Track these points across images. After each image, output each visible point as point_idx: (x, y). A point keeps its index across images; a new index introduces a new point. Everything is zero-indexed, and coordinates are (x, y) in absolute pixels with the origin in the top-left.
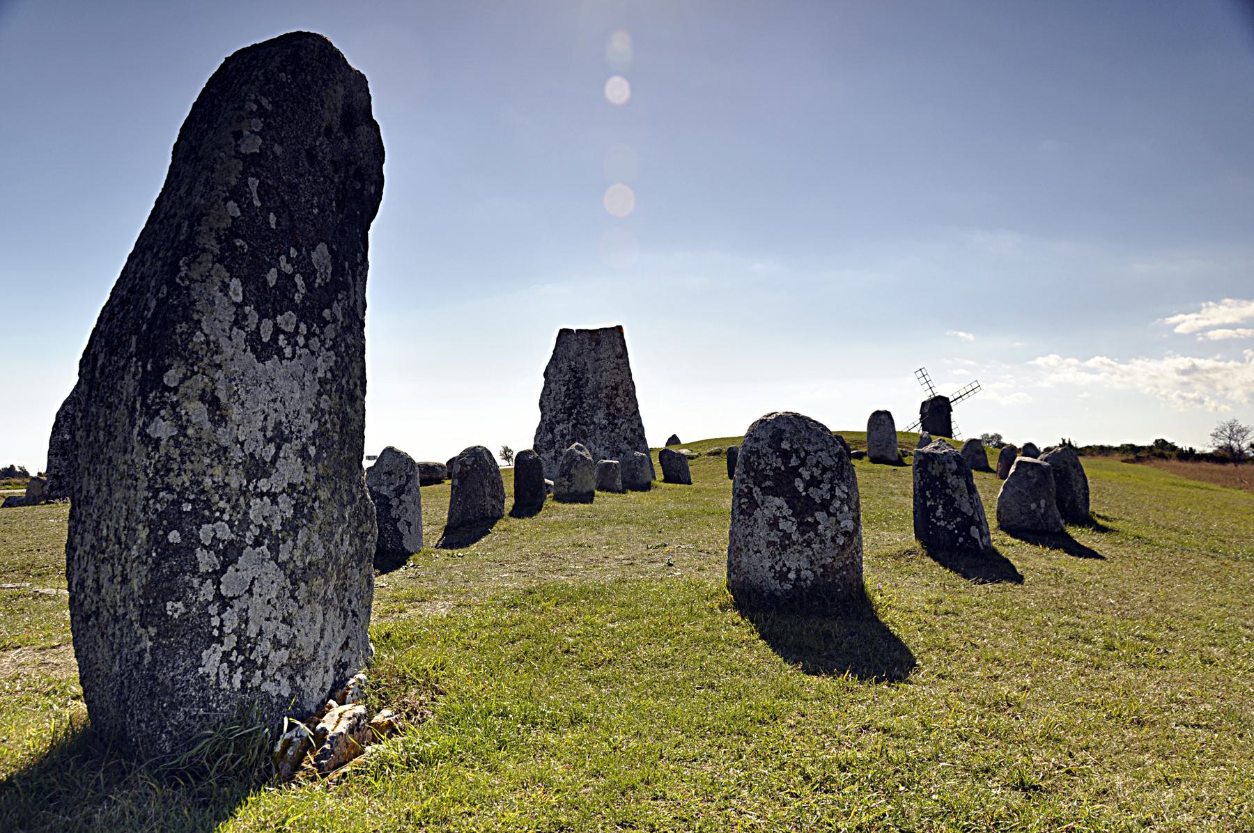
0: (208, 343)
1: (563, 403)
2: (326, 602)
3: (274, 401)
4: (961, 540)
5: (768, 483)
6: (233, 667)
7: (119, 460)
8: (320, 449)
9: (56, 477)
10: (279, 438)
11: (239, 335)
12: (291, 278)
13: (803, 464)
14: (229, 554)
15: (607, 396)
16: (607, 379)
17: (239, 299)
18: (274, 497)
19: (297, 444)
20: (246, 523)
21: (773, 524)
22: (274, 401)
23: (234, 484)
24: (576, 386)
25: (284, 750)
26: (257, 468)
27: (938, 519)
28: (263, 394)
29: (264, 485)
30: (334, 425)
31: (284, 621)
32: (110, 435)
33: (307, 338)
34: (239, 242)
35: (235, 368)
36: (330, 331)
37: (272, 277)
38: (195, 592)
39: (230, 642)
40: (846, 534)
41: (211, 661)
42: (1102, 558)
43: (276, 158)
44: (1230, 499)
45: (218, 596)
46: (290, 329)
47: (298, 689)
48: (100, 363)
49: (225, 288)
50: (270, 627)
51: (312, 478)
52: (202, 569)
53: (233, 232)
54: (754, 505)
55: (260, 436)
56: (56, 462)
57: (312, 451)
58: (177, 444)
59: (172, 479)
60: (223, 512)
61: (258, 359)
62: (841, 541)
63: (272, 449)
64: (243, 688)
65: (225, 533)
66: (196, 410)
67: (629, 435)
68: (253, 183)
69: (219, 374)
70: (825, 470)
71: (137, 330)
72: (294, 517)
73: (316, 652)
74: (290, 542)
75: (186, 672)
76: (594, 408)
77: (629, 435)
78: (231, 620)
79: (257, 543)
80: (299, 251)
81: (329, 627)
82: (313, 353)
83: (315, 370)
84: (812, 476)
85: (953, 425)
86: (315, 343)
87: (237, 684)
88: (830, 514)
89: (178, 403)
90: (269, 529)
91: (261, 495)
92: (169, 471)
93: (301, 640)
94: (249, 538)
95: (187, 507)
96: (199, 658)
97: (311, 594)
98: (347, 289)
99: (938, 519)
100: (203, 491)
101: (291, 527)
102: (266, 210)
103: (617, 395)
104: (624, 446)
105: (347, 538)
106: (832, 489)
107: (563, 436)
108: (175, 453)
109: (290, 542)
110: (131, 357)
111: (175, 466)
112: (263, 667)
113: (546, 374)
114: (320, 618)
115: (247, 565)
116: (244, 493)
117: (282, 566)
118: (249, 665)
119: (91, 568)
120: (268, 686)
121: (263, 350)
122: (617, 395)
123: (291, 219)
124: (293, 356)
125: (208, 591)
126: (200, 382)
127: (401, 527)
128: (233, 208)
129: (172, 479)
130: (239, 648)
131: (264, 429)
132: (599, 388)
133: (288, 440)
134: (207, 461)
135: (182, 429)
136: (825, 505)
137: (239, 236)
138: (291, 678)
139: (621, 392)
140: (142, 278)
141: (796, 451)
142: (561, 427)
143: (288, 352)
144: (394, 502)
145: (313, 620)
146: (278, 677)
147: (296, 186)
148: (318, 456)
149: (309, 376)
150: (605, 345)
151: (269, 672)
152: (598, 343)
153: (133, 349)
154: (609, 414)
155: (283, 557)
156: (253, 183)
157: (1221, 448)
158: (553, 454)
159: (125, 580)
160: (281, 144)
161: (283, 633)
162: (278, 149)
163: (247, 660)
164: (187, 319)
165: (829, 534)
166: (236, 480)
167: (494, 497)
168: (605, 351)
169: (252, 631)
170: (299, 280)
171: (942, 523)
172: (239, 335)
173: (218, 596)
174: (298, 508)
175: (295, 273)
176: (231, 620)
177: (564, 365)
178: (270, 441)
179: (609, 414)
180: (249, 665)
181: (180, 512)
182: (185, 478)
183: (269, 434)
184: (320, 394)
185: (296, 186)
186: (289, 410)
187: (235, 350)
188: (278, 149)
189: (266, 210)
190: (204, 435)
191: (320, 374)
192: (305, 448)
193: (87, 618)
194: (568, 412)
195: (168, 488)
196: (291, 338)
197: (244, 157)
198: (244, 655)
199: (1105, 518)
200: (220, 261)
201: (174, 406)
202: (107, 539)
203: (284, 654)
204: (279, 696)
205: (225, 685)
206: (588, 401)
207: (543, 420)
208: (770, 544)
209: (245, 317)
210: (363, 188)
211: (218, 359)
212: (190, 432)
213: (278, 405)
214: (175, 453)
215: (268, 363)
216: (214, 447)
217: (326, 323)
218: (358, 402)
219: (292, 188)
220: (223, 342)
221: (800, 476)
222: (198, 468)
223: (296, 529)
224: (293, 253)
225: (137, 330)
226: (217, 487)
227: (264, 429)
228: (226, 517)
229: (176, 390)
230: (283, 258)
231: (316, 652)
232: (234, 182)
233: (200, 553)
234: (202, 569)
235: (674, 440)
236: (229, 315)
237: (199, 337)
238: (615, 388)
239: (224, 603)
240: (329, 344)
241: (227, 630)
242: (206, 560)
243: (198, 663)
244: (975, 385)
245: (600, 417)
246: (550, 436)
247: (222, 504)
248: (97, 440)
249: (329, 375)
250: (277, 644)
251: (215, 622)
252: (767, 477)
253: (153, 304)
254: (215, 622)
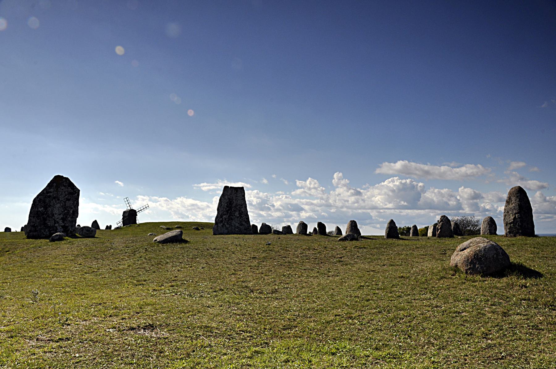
9: (33, 226)
42: (537, 275)
56: (32, 218)
77: (245, 220)
107: (225, 219)
132: (237, 205)
142: (225, 216)
152: (237, 191)
157: (380, 167)
158: (222, 224)
177: (226, 197)
194: (227, 211)
199: (548, 218)
206: (233, 209)
218: (220, 213)
238: (242, 205)
245: (237, 214)
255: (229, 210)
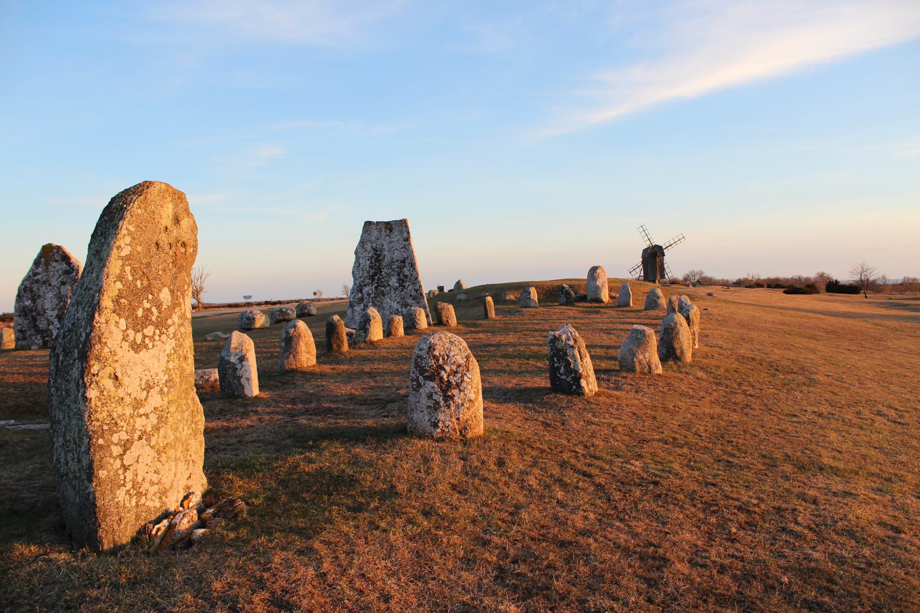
1: (368, 272)
2: (176, 459)
4: (574, 387)
5: (427, 374)
7: (73, 406)
10: (148, 388)
11: (126, 345)
12: (149, 310)
14: (126, 446)
15: (398, 267)
16: (397, 255)
17: (124, 328)
18: (147, 416)
19: (157, 389)
20: (134, 430)
21: (430, 396)
23: (128, 414)
24: (377, 260)
25: (157, 532)
26: (138, 404)
27: (562, 375)
28: (139, 369)
29: (142, 411)
30: (176, 374)
31: (155, 472)
32: (68, 395)
33: (160, 336)
34: (123, 301)
35: (125, 361)
36: (172, 330)
37: (140, 313)
38: (112, 465)
39: (129, 485)
41: (121, 494)
43: (139, 253)
44: (904, 298)
45: (123, 466)
46: (151, 334)
47: (164, 503)
48: (61, 359)
50: (148, 477)
51: (166, 403)
52: (115, 454)
53: (120, 296)
54: (419, 386)
55: (139, 389)
57: (166, 389)
58: (100, 400)
60: (122, 427)
61: (136, 352)
63: (145, 393)
64: (137, 506)
65: (124, 436)
66: (108, 383)
67: (413, 293)
68: (128, 269)
69: (117, 365)
71: (77, 347)
72: (158, 423)
73: (172, 484)
76: (389, 275)
77: (413, 293)
78: (129, 475)
79: (140, 438)
80: (153, 295)
81: (179, 471)
84: (451, 370)
85: (665, 266)
86: (164, 337)
87: (134, 504)
88: (460, 391)
90: (145, 432)
91: (141, 416)
93: (164, 480)
94: (136, 436)
96: (115, 494)
97: (168, 458)
98: (180, 305)
99: (562, 375)
101: (157, 428)
102: (135, 280)
103: (405, 266)
104: (410, 301)
105: (186, 428)
106: (462, 377)
107: (369, 295)
108: (99, 404)
109: (156, 436)
110: (74, 360)
112: (146, 494)
113: (356, 253)
114: (173, 468)
115: (138, 448)
116: (132, 417)
117: (153, 447)
119: (63, 454)
121: (136, 348)
122: (405, 266)
123: (149, 280)
125: (118, 463)
126: (109, 370)
127: (243, 381)
128: (119, 285)
130: (133, 487)
131: (140, 385)
134: (114, 405)
136: (458, 386)
137: (122, 297)
138: (160, 498)
139: (407, 264)
140: (78, 320)
143: (150, 345)
144: (239, 366)
145: (170, 470)
146: (153, 498)
148: (168, 392)
150: (396, 232)
151: (149, 496)
152: (391, 230)
153: (76, 356)
154: (400, 279)
155: (153, 443)
156: (128, 269)
159: (79, 461)
161: (155, 478)
162: (139, 249)
163: (138, 492)
164: (100, 342)
166: (128, 411)
168: (396, 236)
169: (140, 479)
170: (154, 310)
171: (564, 377)
173: (123, 466)
174: (160, 418)
177: (368, 246)
178: (144, 390)
179: (400, 279)
180: (139, 494)
183: (143, 387)
184: (168, 362)
186: (153, 373)
187: (125, 354)
188: (139, 249)
189: (135, 280)
190: (112, 394)
191: (168, 352)
192: (161, 390)
193: (63, 476)
196: (152, 338)
198: (137, 491)
200: (114, 312)
202: (69, 441)
203: (156, 488)
204: (155, 507)
205: (128, 505)
206: (385, 271)
207: (355, 284)
208: (429, 407)
209: (128, 335)
211: (116, 358)
212: (105, 393)
213: (147, 372)
214: (99, 404)
215: (141, 353)
220: (118, 350)
221: (444, 370)
223: (158, 429)
224: (150, 297)
225: (77, 347)
226: (119, 416)
227: (140, 385)
228: (124, 429)
230: (145, 301)
231: (172, 484)
232: (118, 272)
233: (113, 448)
234: (115, 454)
235: (458, 284)
236: (120, 336)
237: (106, 350)
238: (403, 262)
239: (125, 468)
240: (171, 336)
241: (127, 480)
242: (116, 450)
244: (681, 237)
245: (394, 281)
246: (360, 295)
247: (122, 424)
248: (61, 395)
250: (152, 483)
252: (426, 371)
253: (84, 335)
254: (122, 477)
255: (375, 274)
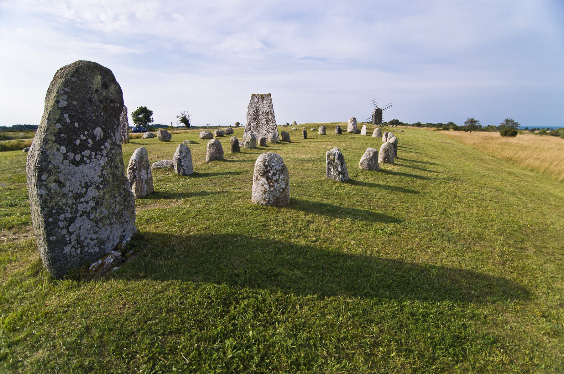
0: (55, 167)
3: (84, 177)
6: (76, 249)
8: (104, 186)
12: (86, 140)
13: (271, 169)
16: (266, 109)
18: (87, 202)
22: (84, 177)
34: (62, 135)
37: (78, 142)
38: (60, 233)
40: (283, 189)
49: (58, 150)
52: (61, 227)
55: (80, 187)
59: (48, 204)
60: (67, 210)
62: (281, 190)
70: (277, 171)
72: (96, 206)
74: (94, 213)
75: (59, 253)
77: (272, 127)
78: (73, 237)
79: (81, 215)
80: (88, 131)
82: (98, 159)
83: (100, 164)
89: (47, 184)
92: (47, 203)
95: (54, 211)
100: (59, 206)
111: (49, 201)
118: (83, 247)
120: (92, 251)
123: (84, 122)
124: (91, 162)
129: (48, 204)
132: (263, 113)
133: (91, 186)
135: (50, 191)
137: (62, 133)
141: (270, 165)
143: (88, 161)
147: (85, 112)
149: (97, 166)
152: (263, 98)
160: (76, 101)
161: (94, 236)
165: (278, 189)
167: (220, 154)
170: (89, 140)
172: (66, 162)
175: (87, 139)
176: (73, 237)
178: (83, 188)
181: (52, 213)
182: (53, 204)
183: (83, 186)
185: (85, 112)
188: (75, 103)
189: (72, 122)
190: (57, 192)
195: (48, 207)
197: (61, 109)
200: (56, 142)
201: (46, 185)
206: (261, 116)
210: (114, 105)
212: (52, 191)
214: (48, 198)
216: (61, 194)
217: (103, 150)
219: (83, 113)
222: (57, 200)
223: (96, 209)
224: (86, 133)
226: (64, 204)
227: (81, 185)
228: (69, 211)
229: (46, 181)
239: (70, 234)
243: (63, 250)
245: (264, 121)
247: (67, 208)
249: (106, 164)
250: (92, 239)
251: (68, 239)
254: (68, 239)
